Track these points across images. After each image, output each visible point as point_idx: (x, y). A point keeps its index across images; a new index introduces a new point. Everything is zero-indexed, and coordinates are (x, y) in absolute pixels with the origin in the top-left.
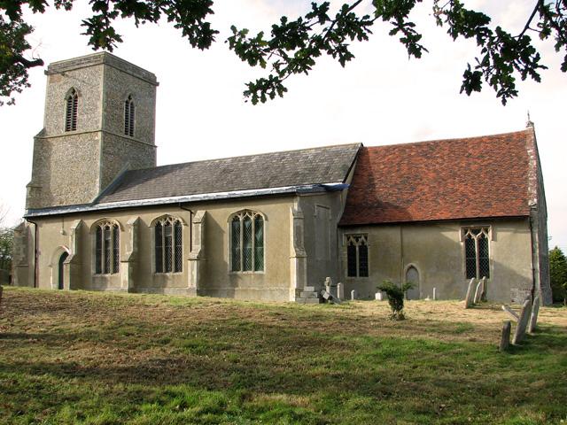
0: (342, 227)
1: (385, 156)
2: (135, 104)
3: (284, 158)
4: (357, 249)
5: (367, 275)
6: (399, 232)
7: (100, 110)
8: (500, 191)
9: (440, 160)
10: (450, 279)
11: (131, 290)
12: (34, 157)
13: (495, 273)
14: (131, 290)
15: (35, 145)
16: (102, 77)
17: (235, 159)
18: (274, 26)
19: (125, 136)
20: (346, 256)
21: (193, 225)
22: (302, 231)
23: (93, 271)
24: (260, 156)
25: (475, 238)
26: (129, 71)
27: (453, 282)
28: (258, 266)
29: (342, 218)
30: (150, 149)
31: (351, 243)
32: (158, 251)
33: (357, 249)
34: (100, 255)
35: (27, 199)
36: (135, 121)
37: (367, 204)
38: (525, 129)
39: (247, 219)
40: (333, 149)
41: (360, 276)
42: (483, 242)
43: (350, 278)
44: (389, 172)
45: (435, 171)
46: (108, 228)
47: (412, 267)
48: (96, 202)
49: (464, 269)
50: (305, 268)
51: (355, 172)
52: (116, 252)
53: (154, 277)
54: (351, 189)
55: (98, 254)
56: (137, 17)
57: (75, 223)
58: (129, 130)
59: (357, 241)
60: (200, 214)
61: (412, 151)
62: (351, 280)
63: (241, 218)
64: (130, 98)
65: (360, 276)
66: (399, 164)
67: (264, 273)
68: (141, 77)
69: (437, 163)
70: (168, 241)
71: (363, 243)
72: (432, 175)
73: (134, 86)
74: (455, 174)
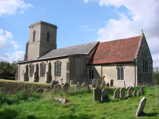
4: (91, 71)
6: (101, 66)
7: (40, 36)
8: (129, 54)
9: (116, 46)
11: (35, 81)
14: (35, 81)
16: (40, 27)
19: (47, 42)
20: (89, 73)
25: (120, 68)
26: (48, 25)
36: (50, 38)
42: (122, 70)
43: (89, 79)
44: (103, 49)
48: (38, 59)
57: (26, 65)
58: (48, 41)
60: (49, 62)
63: (57, 63)
64: (48, 32)
66: (106, 47)
72: (114, 50)
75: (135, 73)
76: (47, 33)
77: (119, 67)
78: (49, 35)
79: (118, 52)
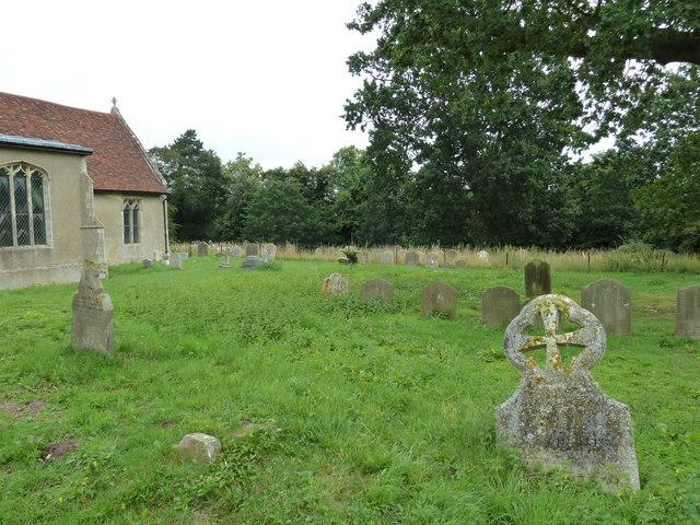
39: (21, 175)
42: (136, 211)
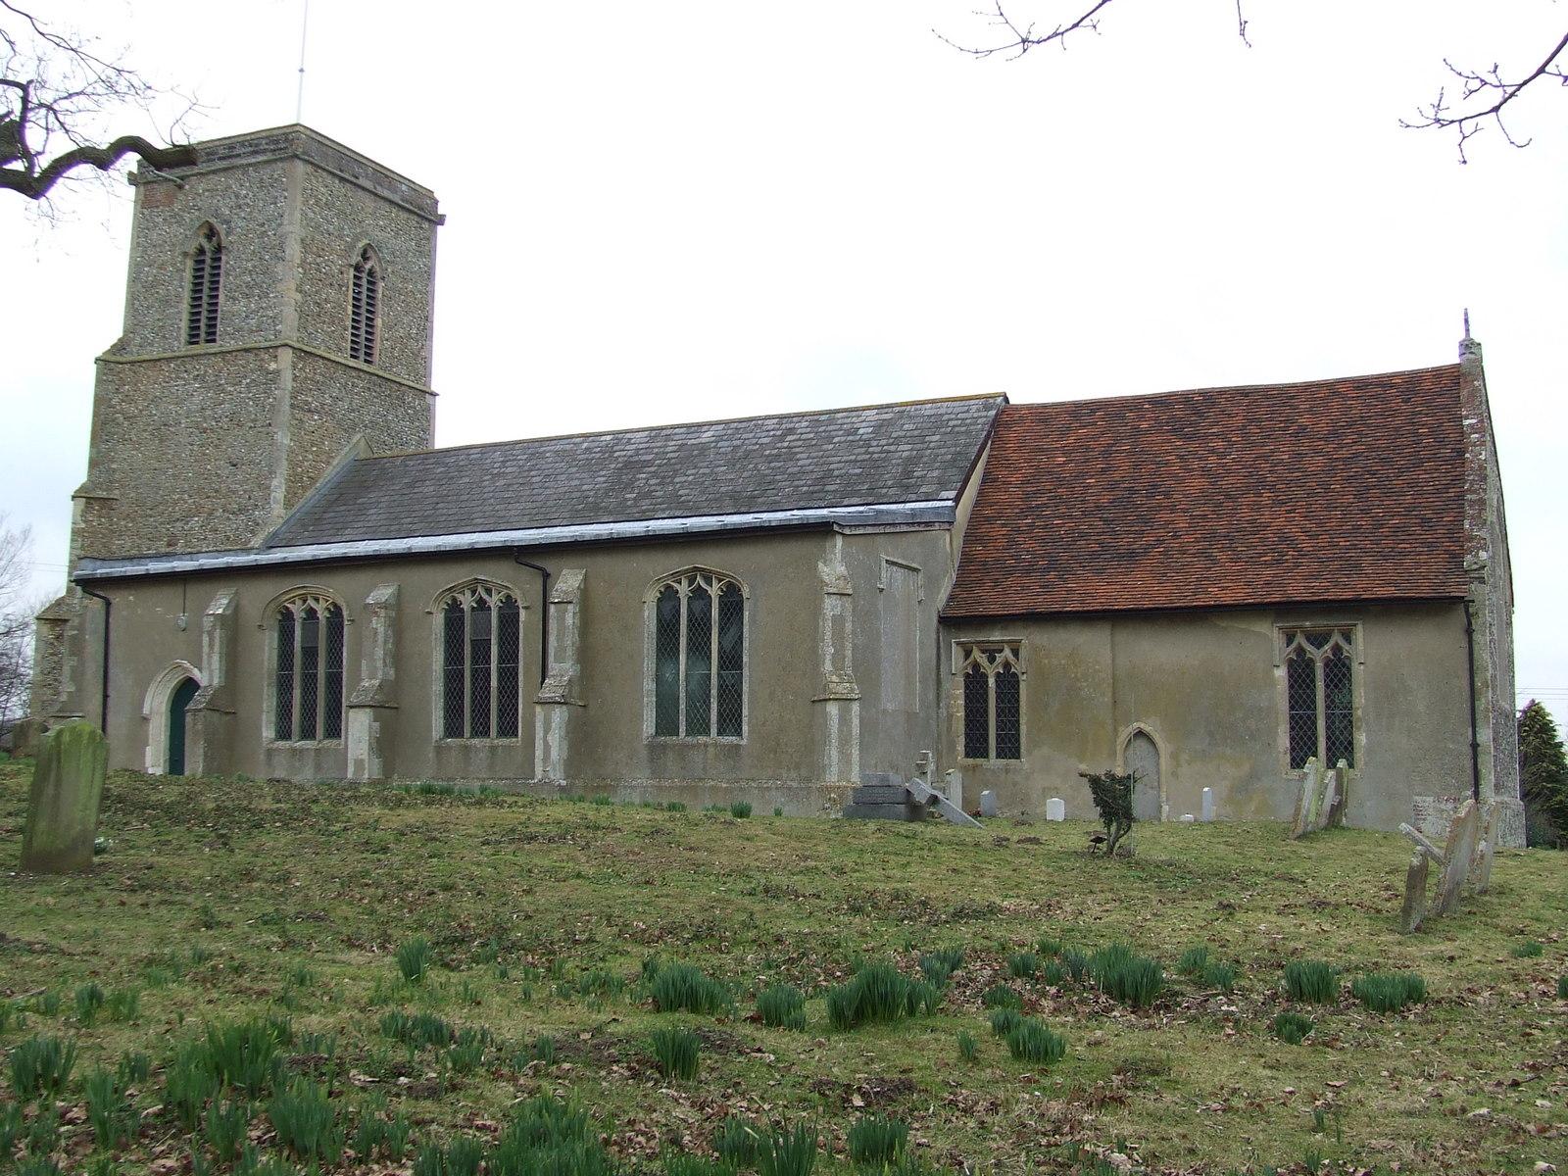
0: (949, 622)
1: (1064, 433)
2: (379, 274)
3: (791, 431)
4: (991, 682)
5: (1015, 754)
10: (1246, 768)
12: (96, 414)
13: (1369, 750)
15: (99, 382)
17: (656, 432)
18: (130, 174)
19: (352, 363)
20: (962, 702)
21: (552, 608)
22: (849, 626)
23: (268, 732)
24: (727, 423)
25: (1319, 656)
26: (362, 181)
27: (1254, 776)
28: (731, 721)
29: (951, 598)
30: (417, 399)
31: (976, 666)
32: (453, 679)
33: (991, 682)
34: (290, 688)
35: (76, 533)
36: (379, 322)
37: (1018, 559)
38: (1456, 360)
39: (699, 594)
40: (928, 410)
41: (998, 756)
42: (1339, 672)
43: (970, 761)
44: (1082, 475)
45: (1205, 472)
46: (311, 613)
47: (1140, 734)
49: (1284, 741)
50: (856, 731)
51: (986, 473)
52: (335, 681)
53: (439, 750)
54: (976, 519)
55: (284, 686)
56: (26, 121)
58: (361, 346)
59: (992, 660)
61: (1141, 418)
62: (975, 768)
63: (683, 589)
65: (998, 756)
66: (1107, 453)
67: (744, 742)
68: (397, 199)
69: (1213, 451)
70: (481, 649)
71: (1007, 665)
72: (1198, 483)
73: (380, 226)
74: (1262, 480)
75: (1466, 706)
76: (356, 259)
77: (1308, 647)
78: (366, 280)
79: (1257, 507)
